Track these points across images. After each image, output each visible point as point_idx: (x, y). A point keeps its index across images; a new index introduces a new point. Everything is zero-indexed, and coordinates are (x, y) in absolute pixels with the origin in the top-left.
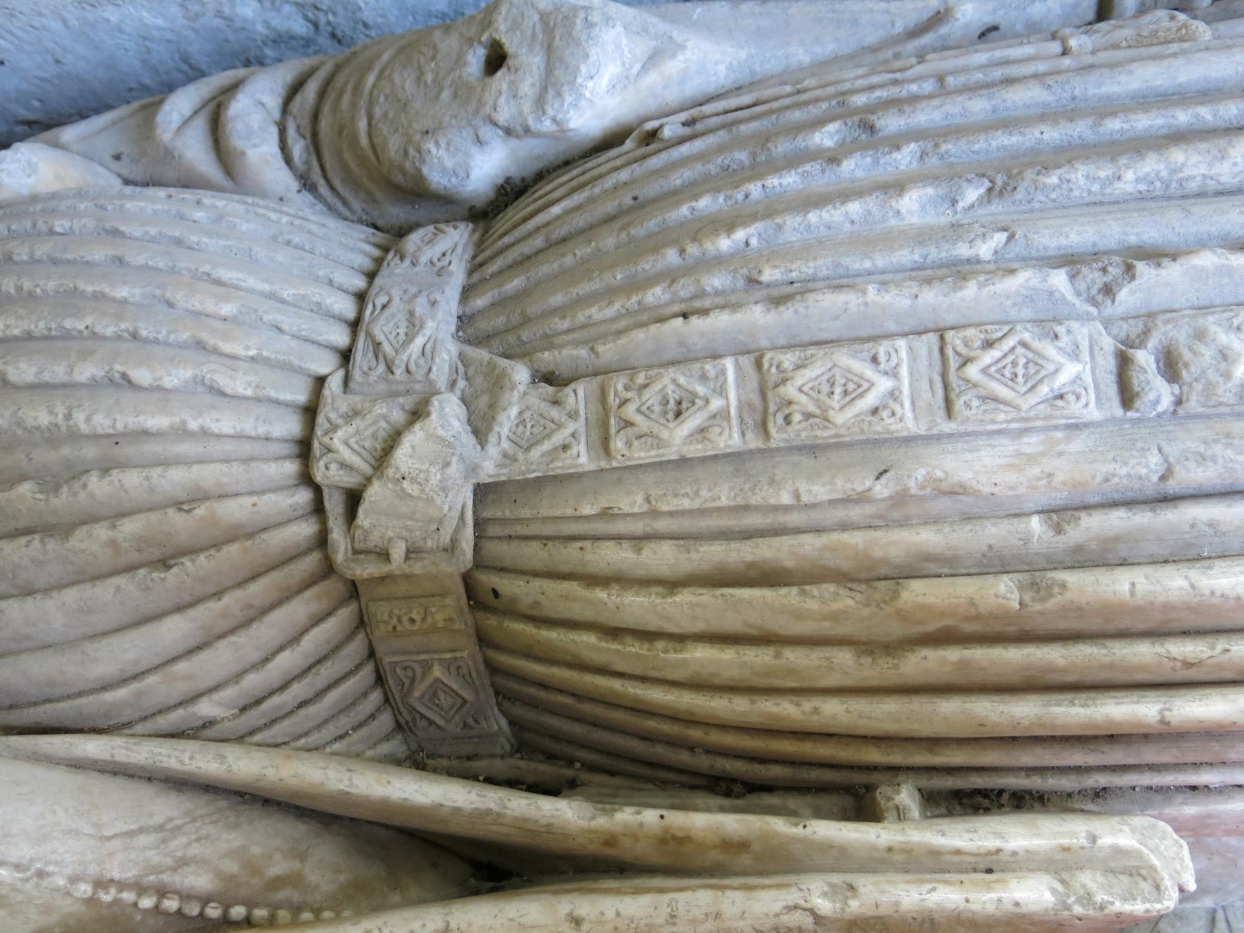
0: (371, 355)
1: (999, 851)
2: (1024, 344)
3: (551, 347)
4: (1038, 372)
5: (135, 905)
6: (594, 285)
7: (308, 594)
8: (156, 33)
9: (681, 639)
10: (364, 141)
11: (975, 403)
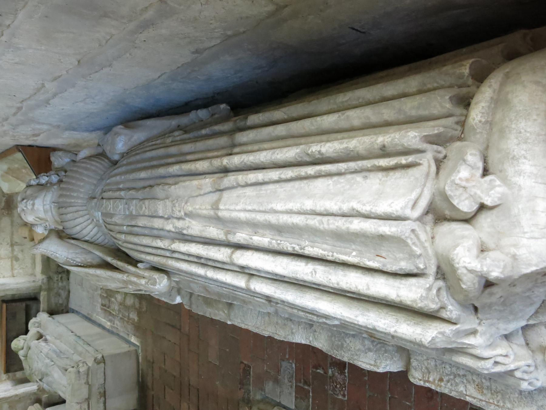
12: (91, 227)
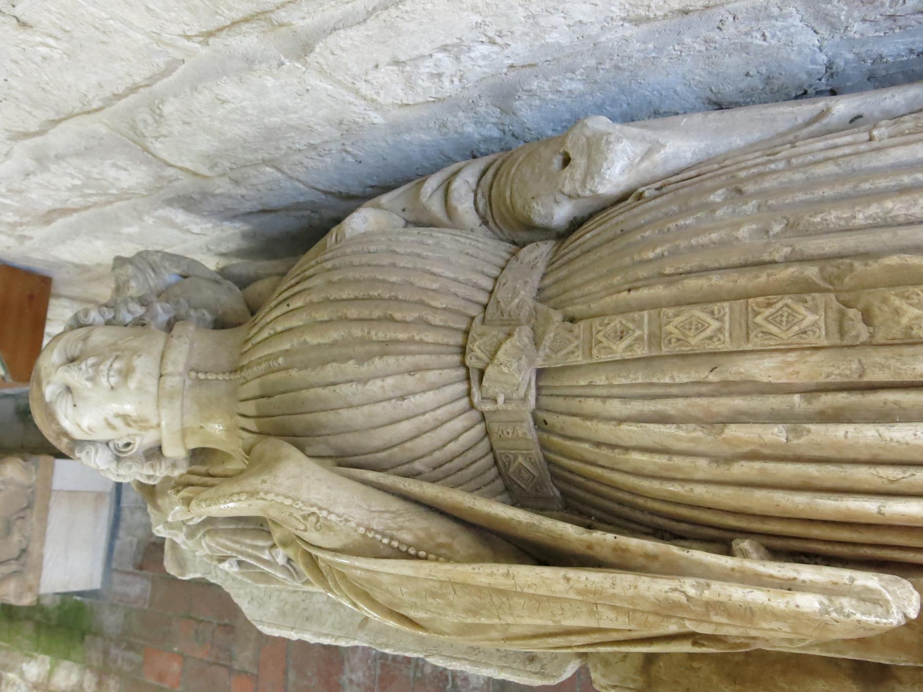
0: (495, 308)
1: (795, 579)
2: (787, 305)
3: (573, 304)
4: (793, 320)
5: (381, 541)
6: (591, 275)
7: (462, 417)
8: (427, 143)
9: (627, 449)
10: (508, 201)
11: (760, 335)
12: (458, 424)
